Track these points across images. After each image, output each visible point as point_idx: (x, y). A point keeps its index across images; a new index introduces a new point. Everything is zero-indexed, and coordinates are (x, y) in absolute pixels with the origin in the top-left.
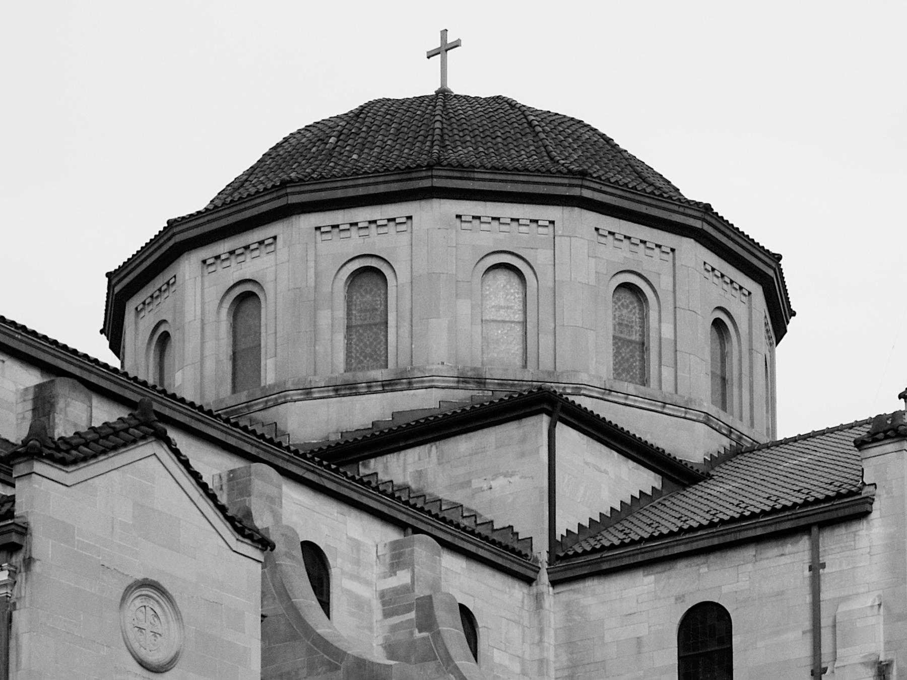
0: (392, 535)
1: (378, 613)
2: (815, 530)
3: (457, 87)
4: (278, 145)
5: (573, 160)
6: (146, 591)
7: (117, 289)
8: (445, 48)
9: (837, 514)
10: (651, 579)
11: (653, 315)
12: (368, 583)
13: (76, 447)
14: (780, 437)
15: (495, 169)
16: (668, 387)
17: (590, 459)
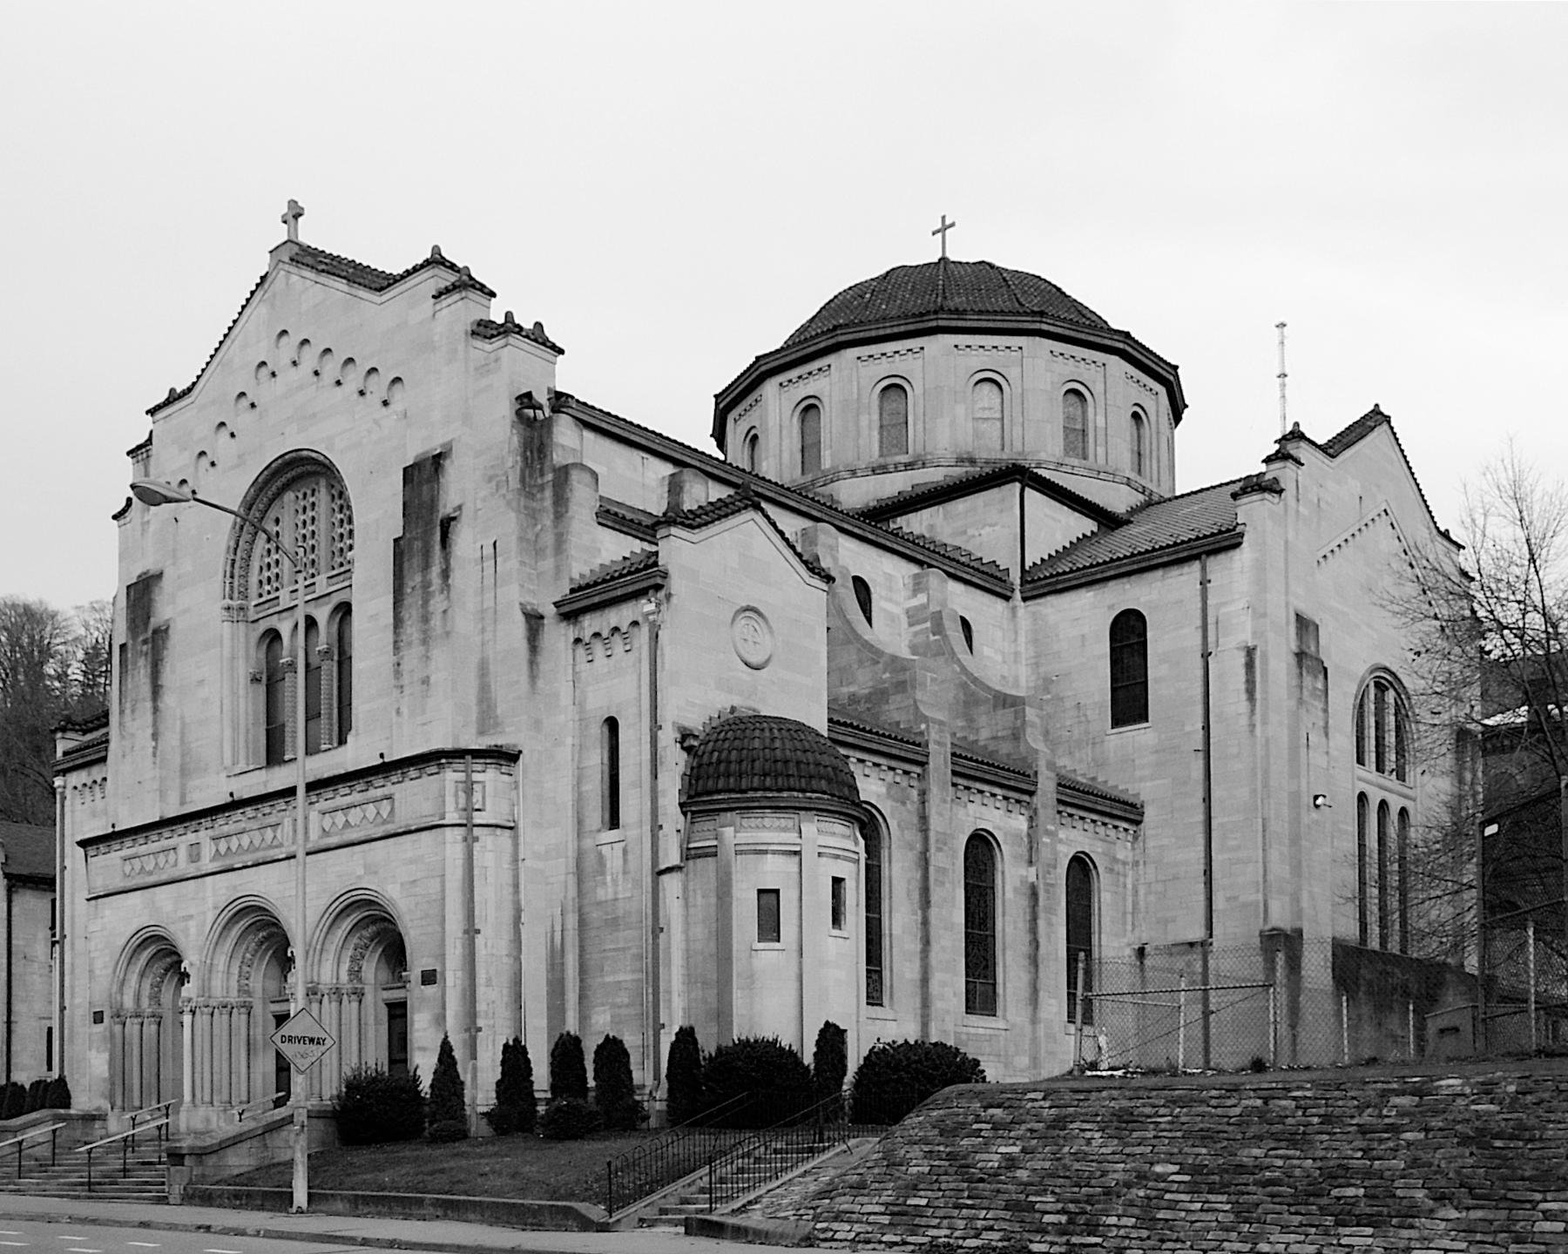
0: (914, 569)
1: (905, 624)
4: (831, 301)
5: (1034, 304)
6: (748, 614)
7: (721, 406)
9: (423, 1049)
10: (1091, 593)
11: (1090, 410)
12: (897, 604)
13: (699, 516)
14: (1178, 493)
15: (980, 312)
16: (1101, 460)
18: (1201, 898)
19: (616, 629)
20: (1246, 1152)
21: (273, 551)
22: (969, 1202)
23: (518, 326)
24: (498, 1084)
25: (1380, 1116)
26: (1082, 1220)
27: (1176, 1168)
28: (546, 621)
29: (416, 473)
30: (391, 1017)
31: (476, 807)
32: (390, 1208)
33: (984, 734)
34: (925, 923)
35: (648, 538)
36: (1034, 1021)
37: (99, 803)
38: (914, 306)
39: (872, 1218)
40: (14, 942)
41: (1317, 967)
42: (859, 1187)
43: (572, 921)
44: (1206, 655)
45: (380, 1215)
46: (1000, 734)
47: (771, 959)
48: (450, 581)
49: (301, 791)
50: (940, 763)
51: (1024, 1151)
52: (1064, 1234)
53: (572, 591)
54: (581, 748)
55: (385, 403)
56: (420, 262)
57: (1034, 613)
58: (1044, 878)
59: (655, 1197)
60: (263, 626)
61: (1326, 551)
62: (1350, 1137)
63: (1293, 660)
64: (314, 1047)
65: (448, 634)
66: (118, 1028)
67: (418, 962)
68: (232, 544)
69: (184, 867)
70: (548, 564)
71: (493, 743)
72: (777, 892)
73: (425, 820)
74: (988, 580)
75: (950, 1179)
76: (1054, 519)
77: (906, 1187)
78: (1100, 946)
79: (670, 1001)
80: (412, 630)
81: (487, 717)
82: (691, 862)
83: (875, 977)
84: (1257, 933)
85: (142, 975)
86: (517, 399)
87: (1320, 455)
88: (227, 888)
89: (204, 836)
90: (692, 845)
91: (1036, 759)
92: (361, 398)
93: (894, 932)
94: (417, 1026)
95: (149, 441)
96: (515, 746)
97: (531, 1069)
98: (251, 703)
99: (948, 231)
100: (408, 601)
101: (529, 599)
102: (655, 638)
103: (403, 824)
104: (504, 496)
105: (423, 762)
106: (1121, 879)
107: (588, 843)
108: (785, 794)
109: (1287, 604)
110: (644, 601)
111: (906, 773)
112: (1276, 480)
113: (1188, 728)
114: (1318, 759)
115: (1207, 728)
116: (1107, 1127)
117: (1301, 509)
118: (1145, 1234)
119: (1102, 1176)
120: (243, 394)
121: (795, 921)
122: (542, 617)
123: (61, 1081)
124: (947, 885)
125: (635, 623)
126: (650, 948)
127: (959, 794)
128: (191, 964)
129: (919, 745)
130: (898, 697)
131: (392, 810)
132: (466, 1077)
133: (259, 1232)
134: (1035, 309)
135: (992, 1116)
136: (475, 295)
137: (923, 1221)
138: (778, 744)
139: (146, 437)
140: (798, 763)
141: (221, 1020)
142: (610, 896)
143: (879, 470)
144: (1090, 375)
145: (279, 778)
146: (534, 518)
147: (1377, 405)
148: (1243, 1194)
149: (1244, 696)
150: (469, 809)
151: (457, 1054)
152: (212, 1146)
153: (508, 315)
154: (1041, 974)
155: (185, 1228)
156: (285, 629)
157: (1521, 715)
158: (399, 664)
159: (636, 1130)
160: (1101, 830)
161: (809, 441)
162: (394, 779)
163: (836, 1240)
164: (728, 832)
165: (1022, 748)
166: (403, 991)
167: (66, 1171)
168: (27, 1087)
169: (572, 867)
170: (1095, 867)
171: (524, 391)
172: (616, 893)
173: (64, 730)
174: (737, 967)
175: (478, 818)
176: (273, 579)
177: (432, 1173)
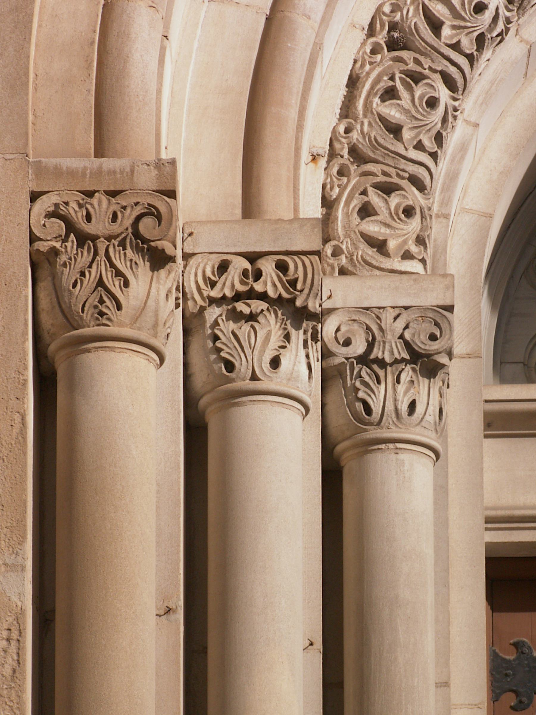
35: (114, 275)
83: (357, 186)
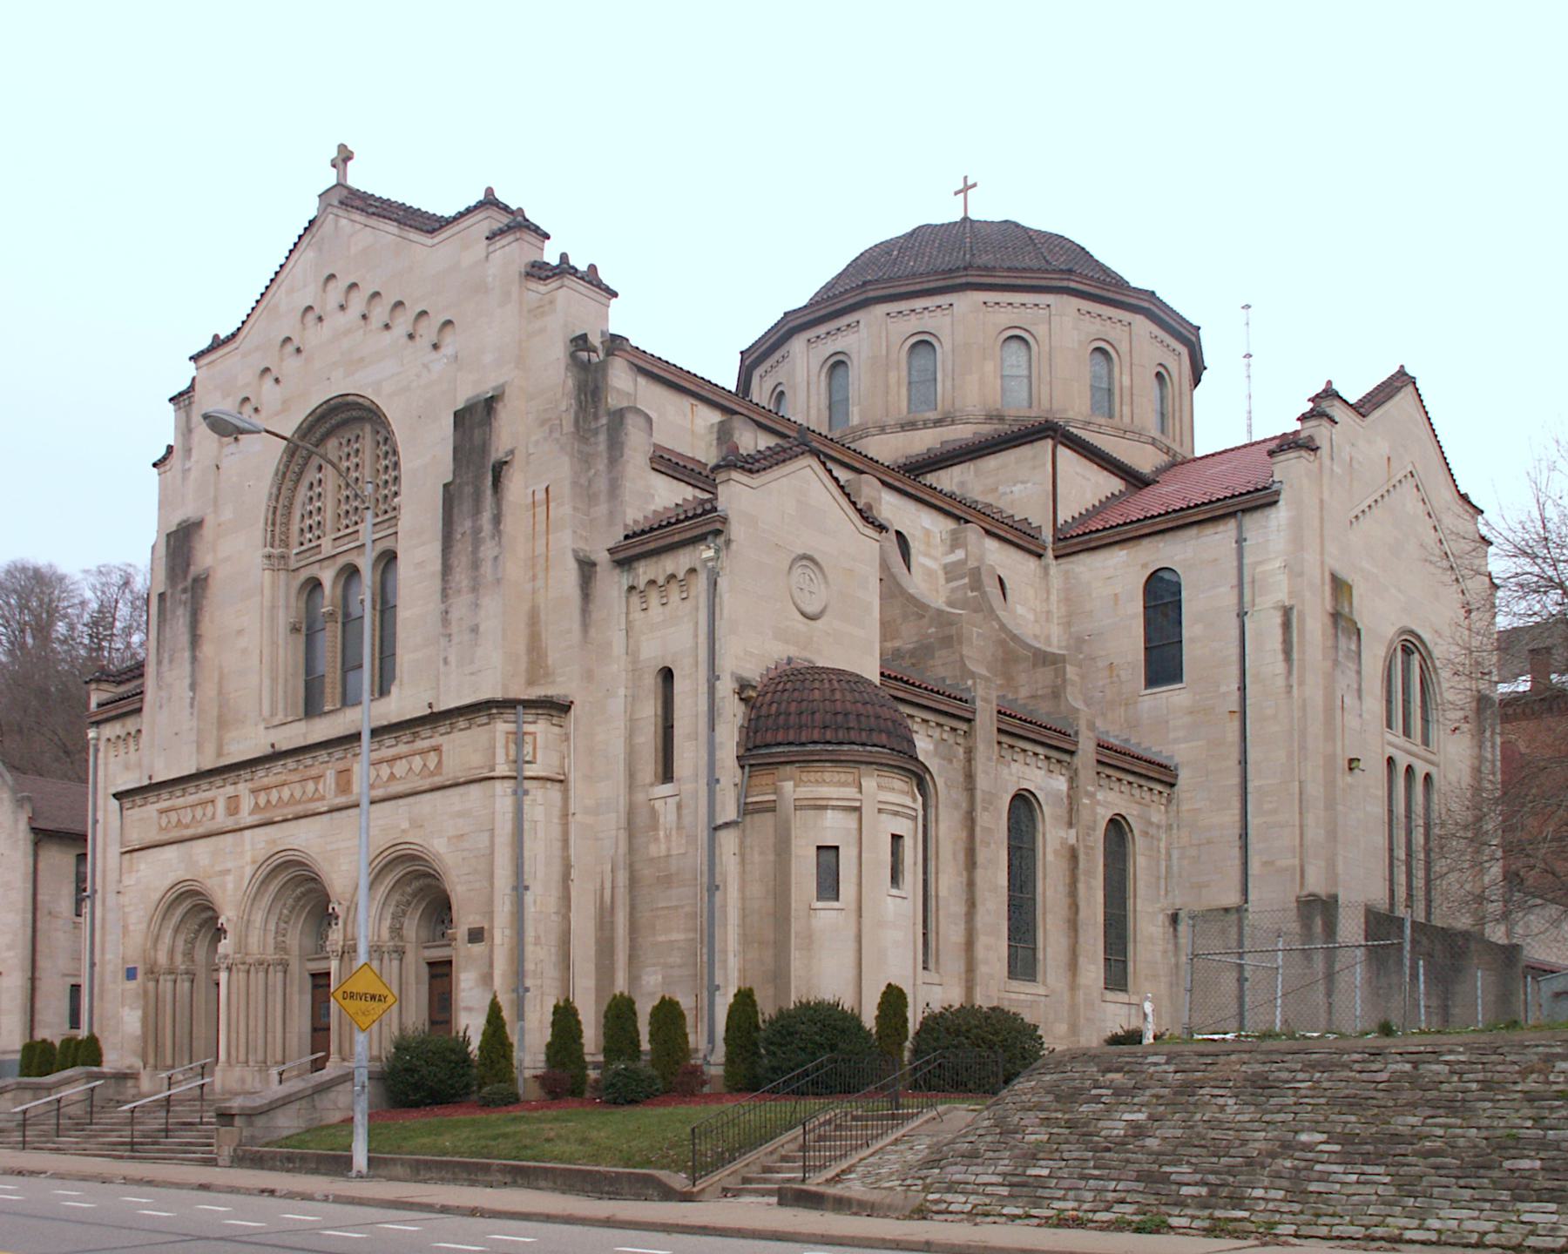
0: (950, 525)
1: (942, 581)
2: (1239, 514)
3: (974, 215)
4: (857, 258)
5: (1060, 262)
6: (805, 562)
7: (747, 362)
8: (966, 188)
9: (469, 1009)
10: (1125, 552)
11: (1116, 370)
12: (935, 559)
13: (758, 461)
14: (1198, 454)
15: (1009, 269)
16: (1127, 419)
17: (1078, 469)
18: (1237, 863)
19: (673, 576)
20: (1400, 1120)
21: (315, 498)
22: (1096, 1172)
23: (573, 268)
24: (549, 1046)
25: (1547, 1082)
26: (1224, 1192)
27: (1324, 1137)
28: (598, 568)
29: (467, 416)
30: (315, 987)
31: (527, 758)
32: (454, 1173)
33: (1024, 693)
34: (971, 884)
36: (1073, 987)
37: (133, 756)
38: (942, 263)
39: (989, 1189)
40: (40, 898)
41: (1351, 928)
42: (972, 1156)
43: (622, 878)
44: (1242, 615)
45: (443, 1180)
46: (1039, 693)
47: (829, 919)
48: (502, 527)
49: (366, 736)
50: (986, 721)
51: (1151, 1118)
52: (1205, 1207)
53: (627, 537)
54: (633, 700)
55: (436, 347)
56: (473, 203)
57: (1067, 572)
58: (1084, 840)
59: (737, 1165)
60: (304, 575)
61: (1357, 511)
62: (1516, 1104)
63: (1328, 621)
64: (375, 1004)
65: (498, 581)
66: (151, 985)
67: (465, 919)
68: (275, 491)
69: (222, 820)
70: (602, 509)
71: (543, 694)
72: (837, 848)
73: (474, 772)
74: (1019, 537)
75: (1072, 1147)
76: (1084, 477)
77: (1024, 1156)
78: (1135, 911)
79: (725, 961)
80: (461, 577)
81: (537, 664)
82: (748, 818)
84: (1294, 899)
85: (177, 930)
86: (572, 341)
87: (1351, 414)
88: (266, 842)
89: (243, 788)
90: (750, 800)
91: (1077, 719)
92: (410, 343)
93: (940, 894)
94: (463, 985)
95: (192, 387)
96: (566, 696)
97: (581, 1031)
98: (289, 653)
99: (969, 192)
100: (457, 547)
101: (581, 545)
102: (713, 585)
103: (451, 776)
104: (557, 440)
105: (473, 712)
106: (1155, 843)
107: (640, 797)
108: (845, 748)
109: (1322, 563)
110: (703, 547)
111: (953, 730)
112: (1311, 438)
113: (1223, 689)
114: (1352, 721)
115: (1243, 688)
116: (1243, 1093)
117: (1335, 468)
118: (1296, 1207)
119: (1241, 1145)
120: (288, 339)
121: (854, 880)
122: (594, 564)
123: (93, 1041)
124: (993, 846)
125: (693, 571)
126: (705, 905)
127: (1102, 782)
128: (228, 920)
129: (966, 702)
130: (944, 652)
131: (440, 762)
132: (514, 1039)
133: (327, 1196)
134: (1063, 267)
135: (1112, 1081)
136: (530, 237)
137: (1047, 1193)
138: (838, 695)
139: (188, 383)
140: (858, 715)
141: (258, 978)
142: (663, 853)
143: (909, 426)
144: (1116, 334)
145: (322, 729)
146: (587, 462)
147: (1402, 367)
148: (1404, 1165)
149: (1281, 657)
150: (519, 762)
151: (505, 1014)
152: (261, 1106)
153: (564, 257)
154: (1081, 939)
155: (248, 1192)
156: (327, 576)
157: (1523, 685)
158: (447, 612)
159: (695, 1096)
160: (1136, 792)
161: (836, 397)
162: (442, 730)
163: (951, 1213)
164: (788, 786)
165: (1063, 708)
166: (447, 949)
167: (104, 1130)
168: (57, 1044)
169: (623, 822)
170: (1131, 831)
171: (578, 333)
172: (669, 849)
173: (98, 680)
174: (795, 927)
175: (530, 771)
176: (315, 526)
177: (495, 1138)
